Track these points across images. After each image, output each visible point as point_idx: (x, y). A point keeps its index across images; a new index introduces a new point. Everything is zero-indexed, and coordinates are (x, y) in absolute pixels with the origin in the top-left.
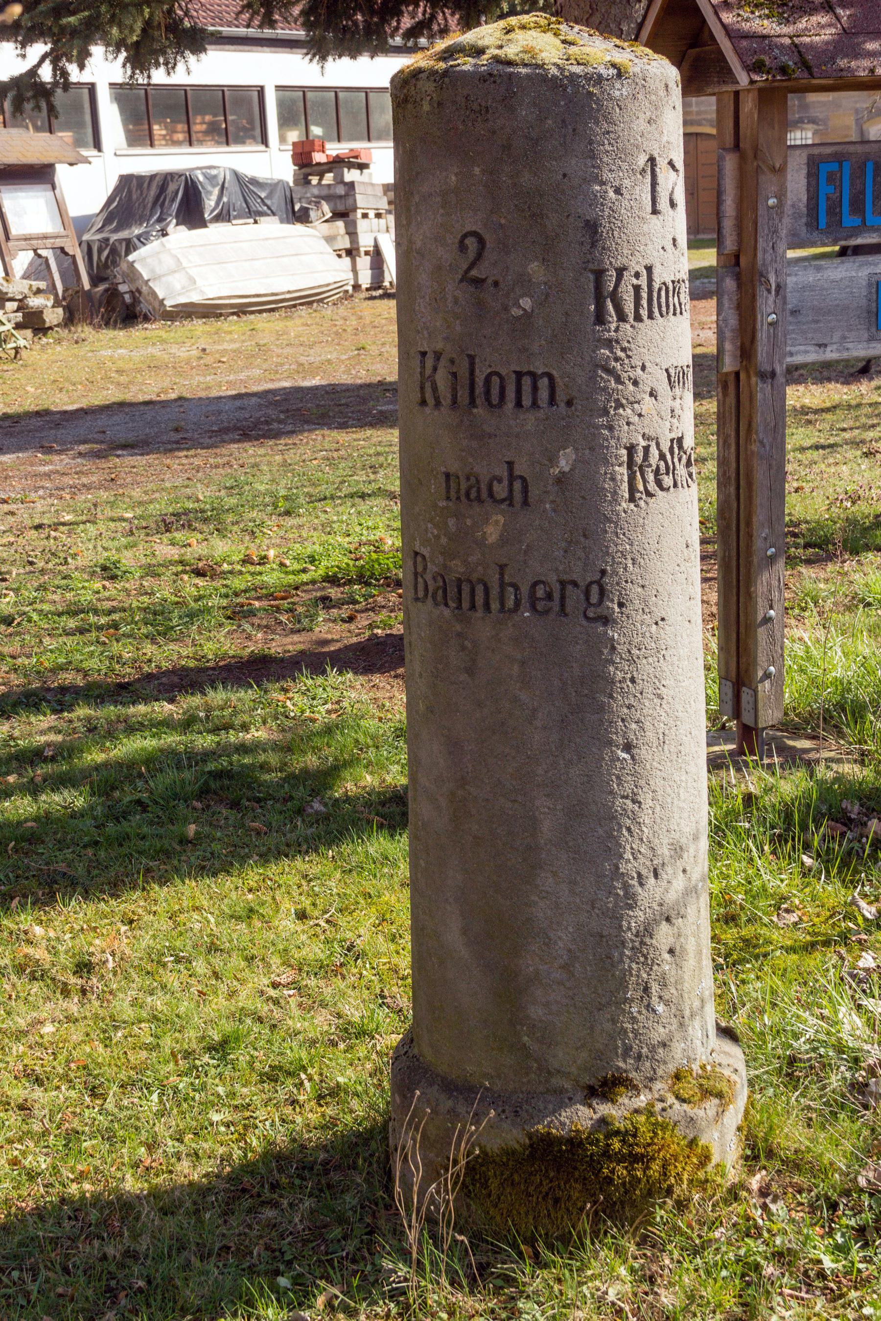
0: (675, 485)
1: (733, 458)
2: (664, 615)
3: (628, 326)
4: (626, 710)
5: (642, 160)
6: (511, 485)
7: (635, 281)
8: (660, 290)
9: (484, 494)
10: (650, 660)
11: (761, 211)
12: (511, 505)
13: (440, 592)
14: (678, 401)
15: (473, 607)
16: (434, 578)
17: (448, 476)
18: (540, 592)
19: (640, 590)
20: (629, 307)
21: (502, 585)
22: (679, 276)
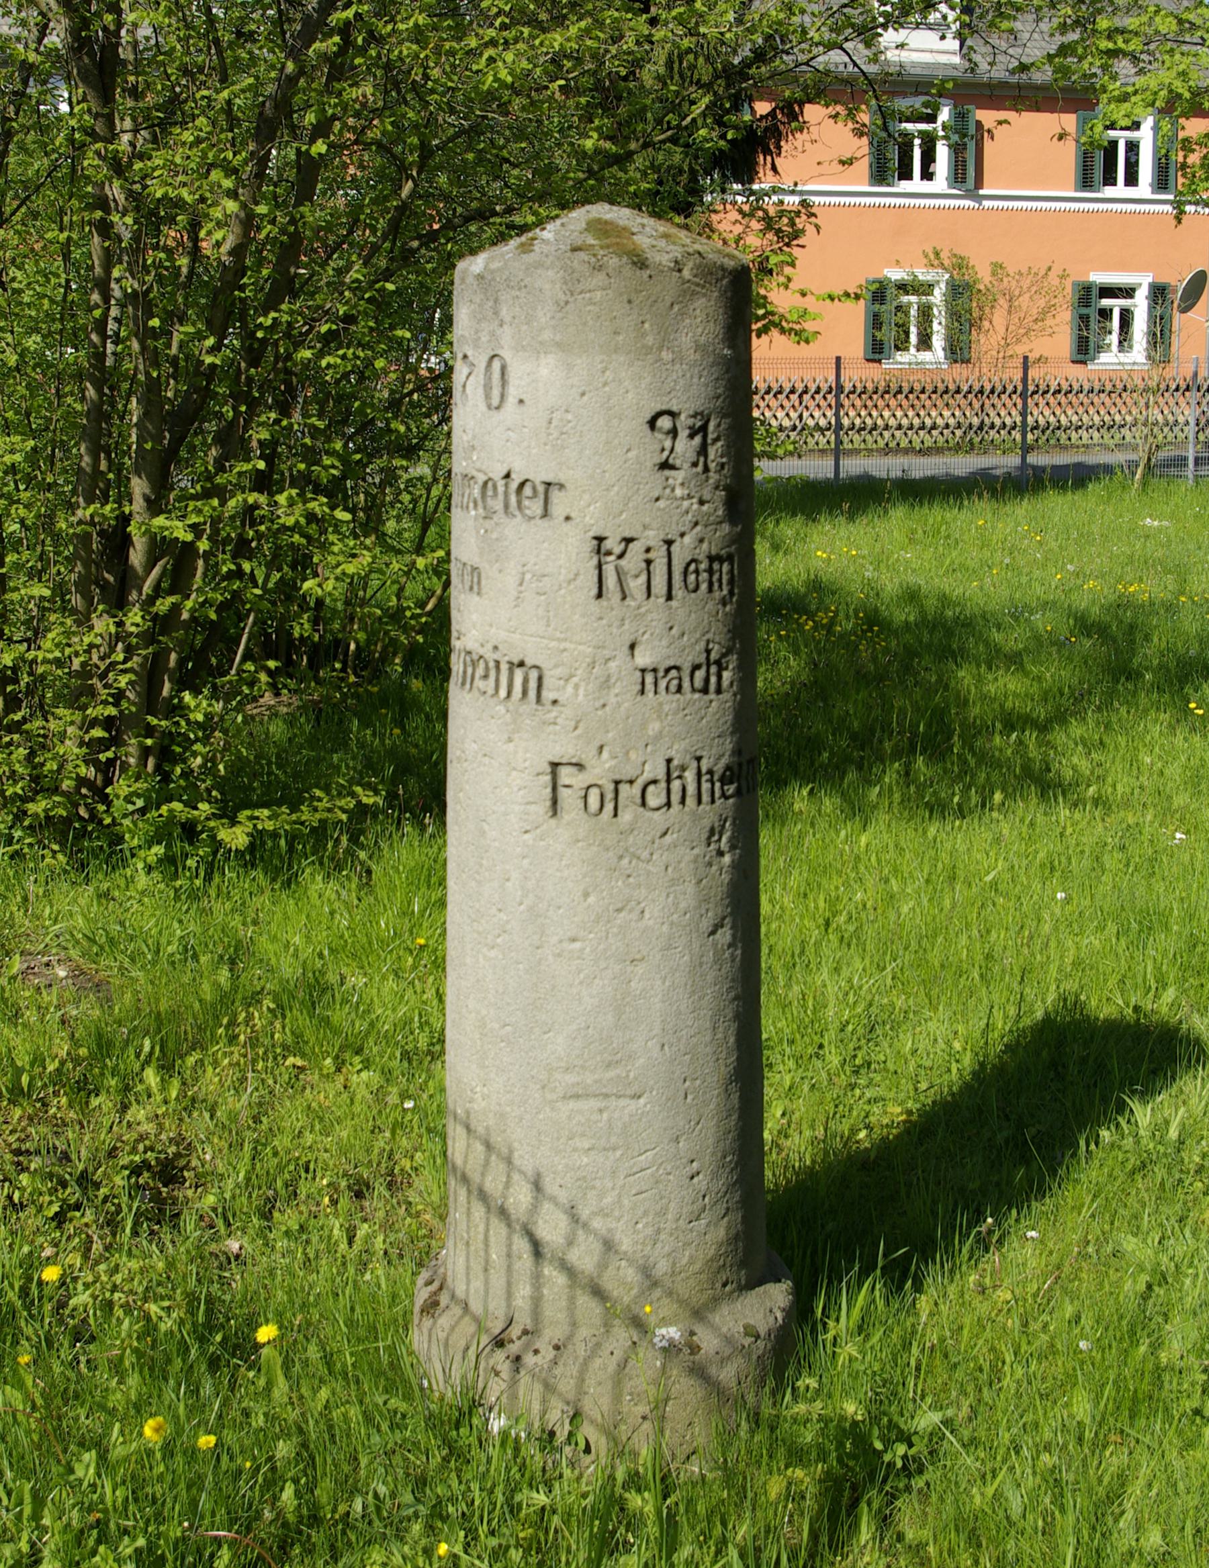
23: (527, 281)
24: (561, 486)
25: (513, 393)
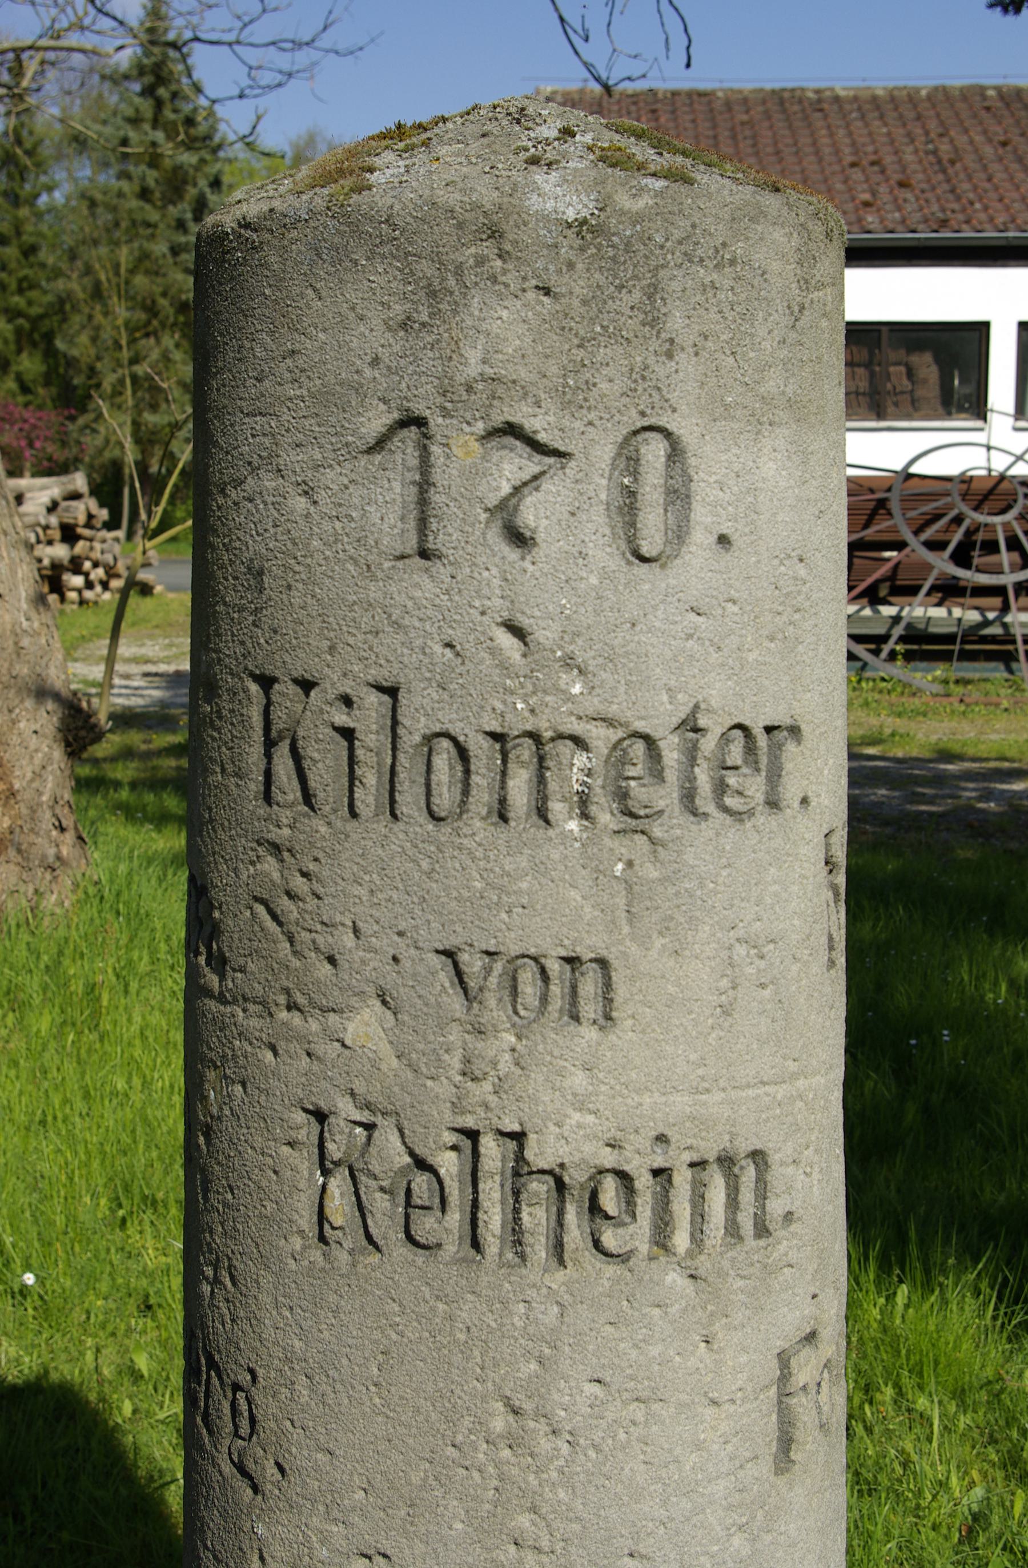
23: (739, 248)
24: (795, 731)
25: (704, 522)
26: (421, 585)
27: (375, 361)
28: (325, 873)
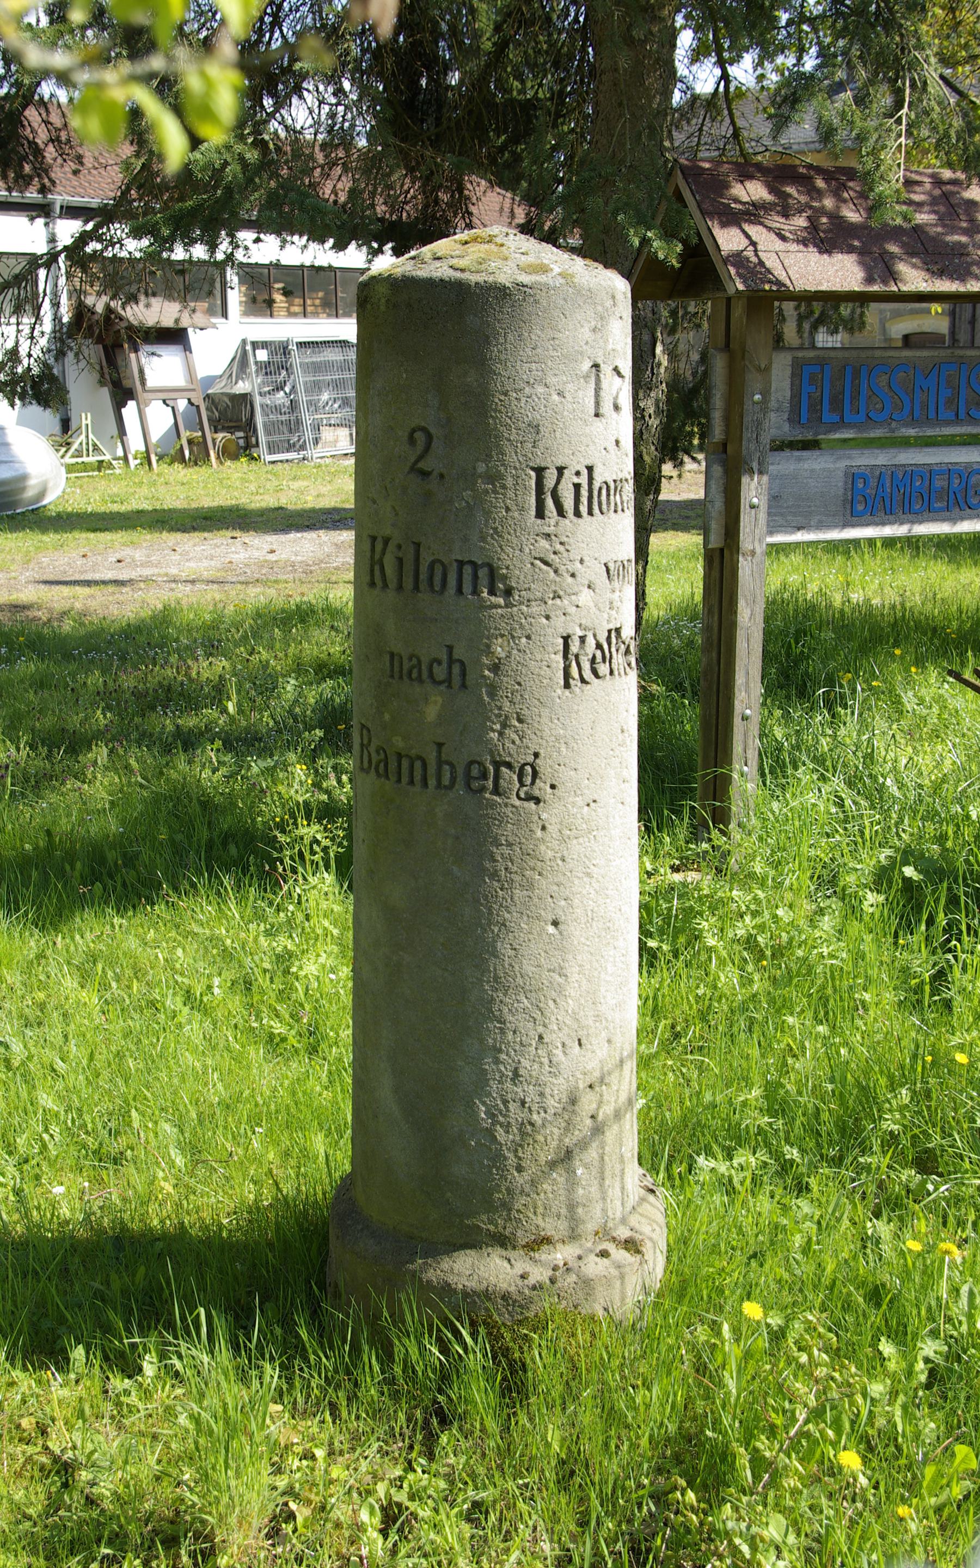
0: (611, 673)
1: (716, 625)
2: (596, 797)
3: (567, 521)
4: (555, 888)
5: (586, 365)
6: (450, 667)
7: (576, 480)
8: (600, 489)
9: (425, 674)
10: (581, 840)
11: (748, 406)
12: (450, 687)
13: (382, 765)
14: (617, 593)
15: (412, 782)
16: (378, 752)
17: (392, 655)
18: (475, 771)
19: (572, 773)
20: (569, 504)
21: (440, 763)
22: (621, 476)
26: (598, 424)
27: (587, 343)
28: (572, 541)
